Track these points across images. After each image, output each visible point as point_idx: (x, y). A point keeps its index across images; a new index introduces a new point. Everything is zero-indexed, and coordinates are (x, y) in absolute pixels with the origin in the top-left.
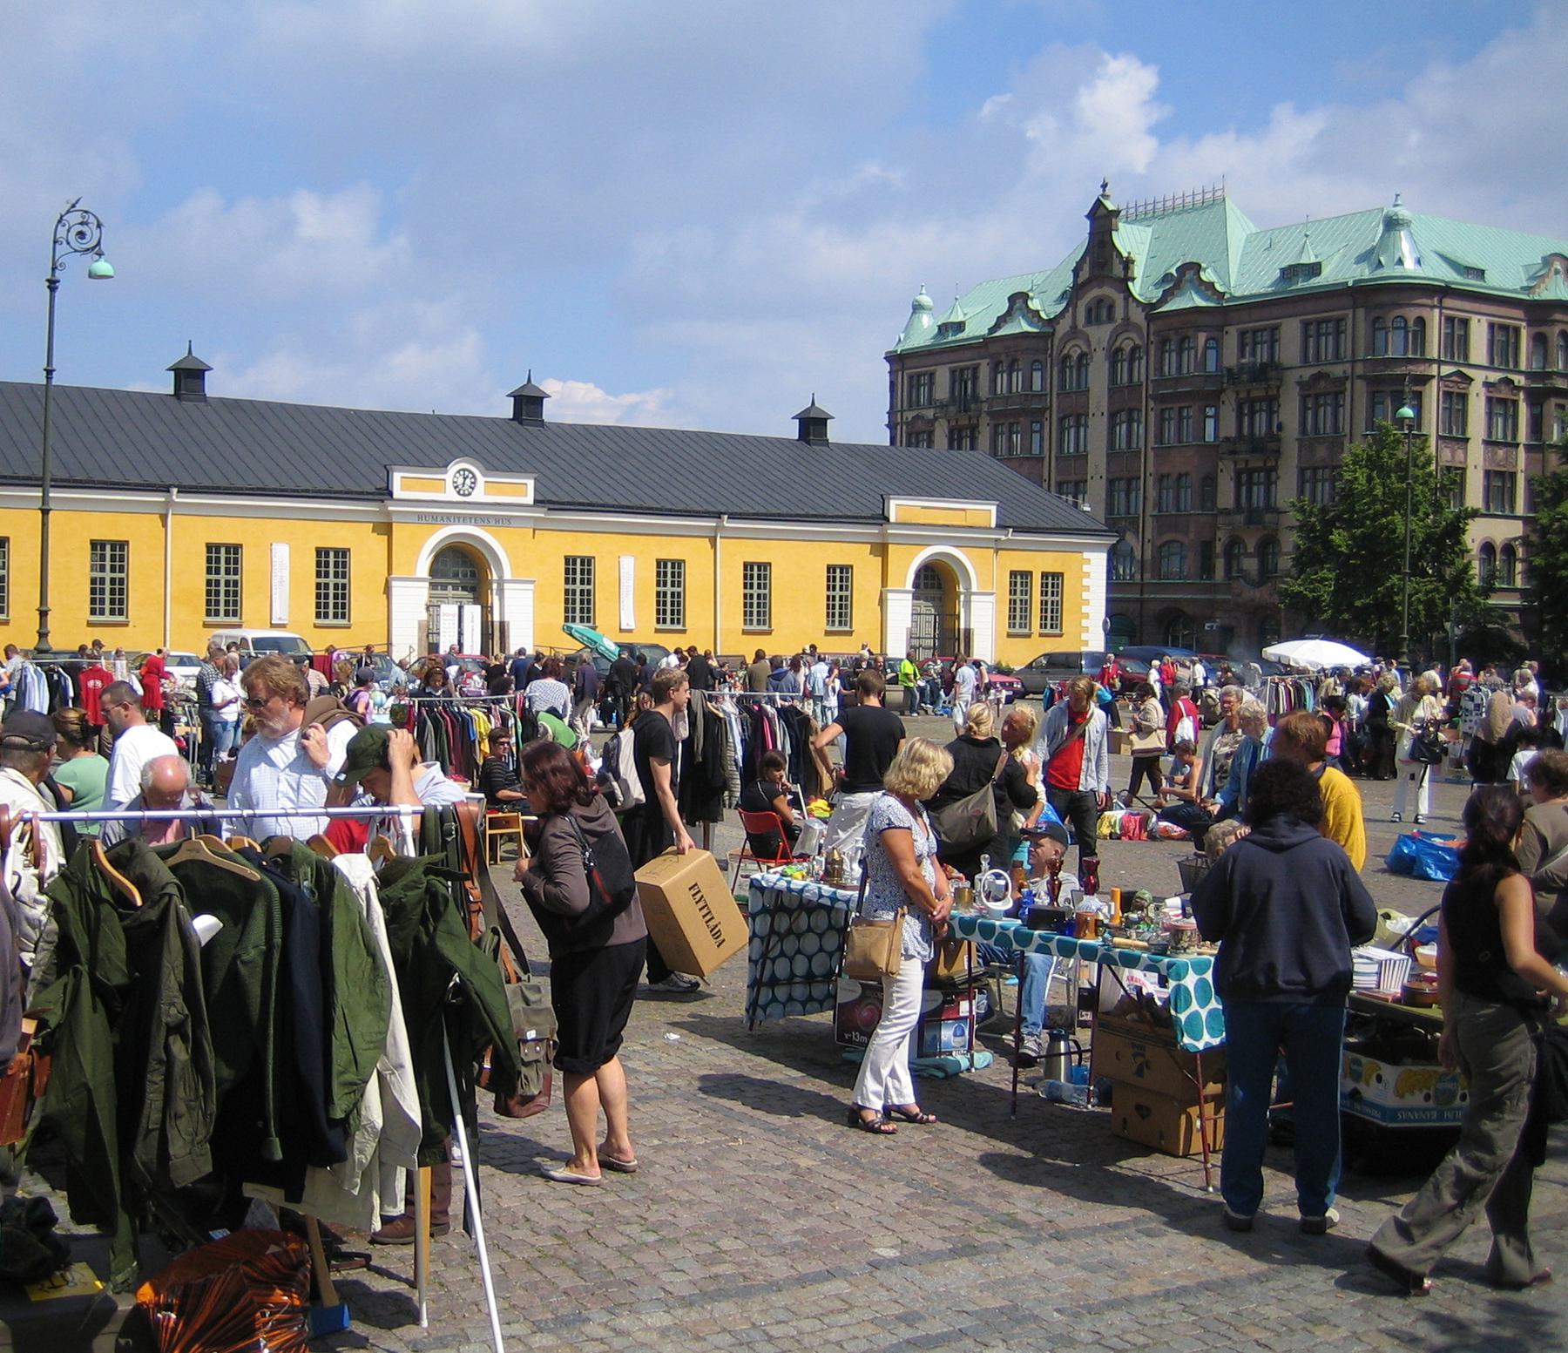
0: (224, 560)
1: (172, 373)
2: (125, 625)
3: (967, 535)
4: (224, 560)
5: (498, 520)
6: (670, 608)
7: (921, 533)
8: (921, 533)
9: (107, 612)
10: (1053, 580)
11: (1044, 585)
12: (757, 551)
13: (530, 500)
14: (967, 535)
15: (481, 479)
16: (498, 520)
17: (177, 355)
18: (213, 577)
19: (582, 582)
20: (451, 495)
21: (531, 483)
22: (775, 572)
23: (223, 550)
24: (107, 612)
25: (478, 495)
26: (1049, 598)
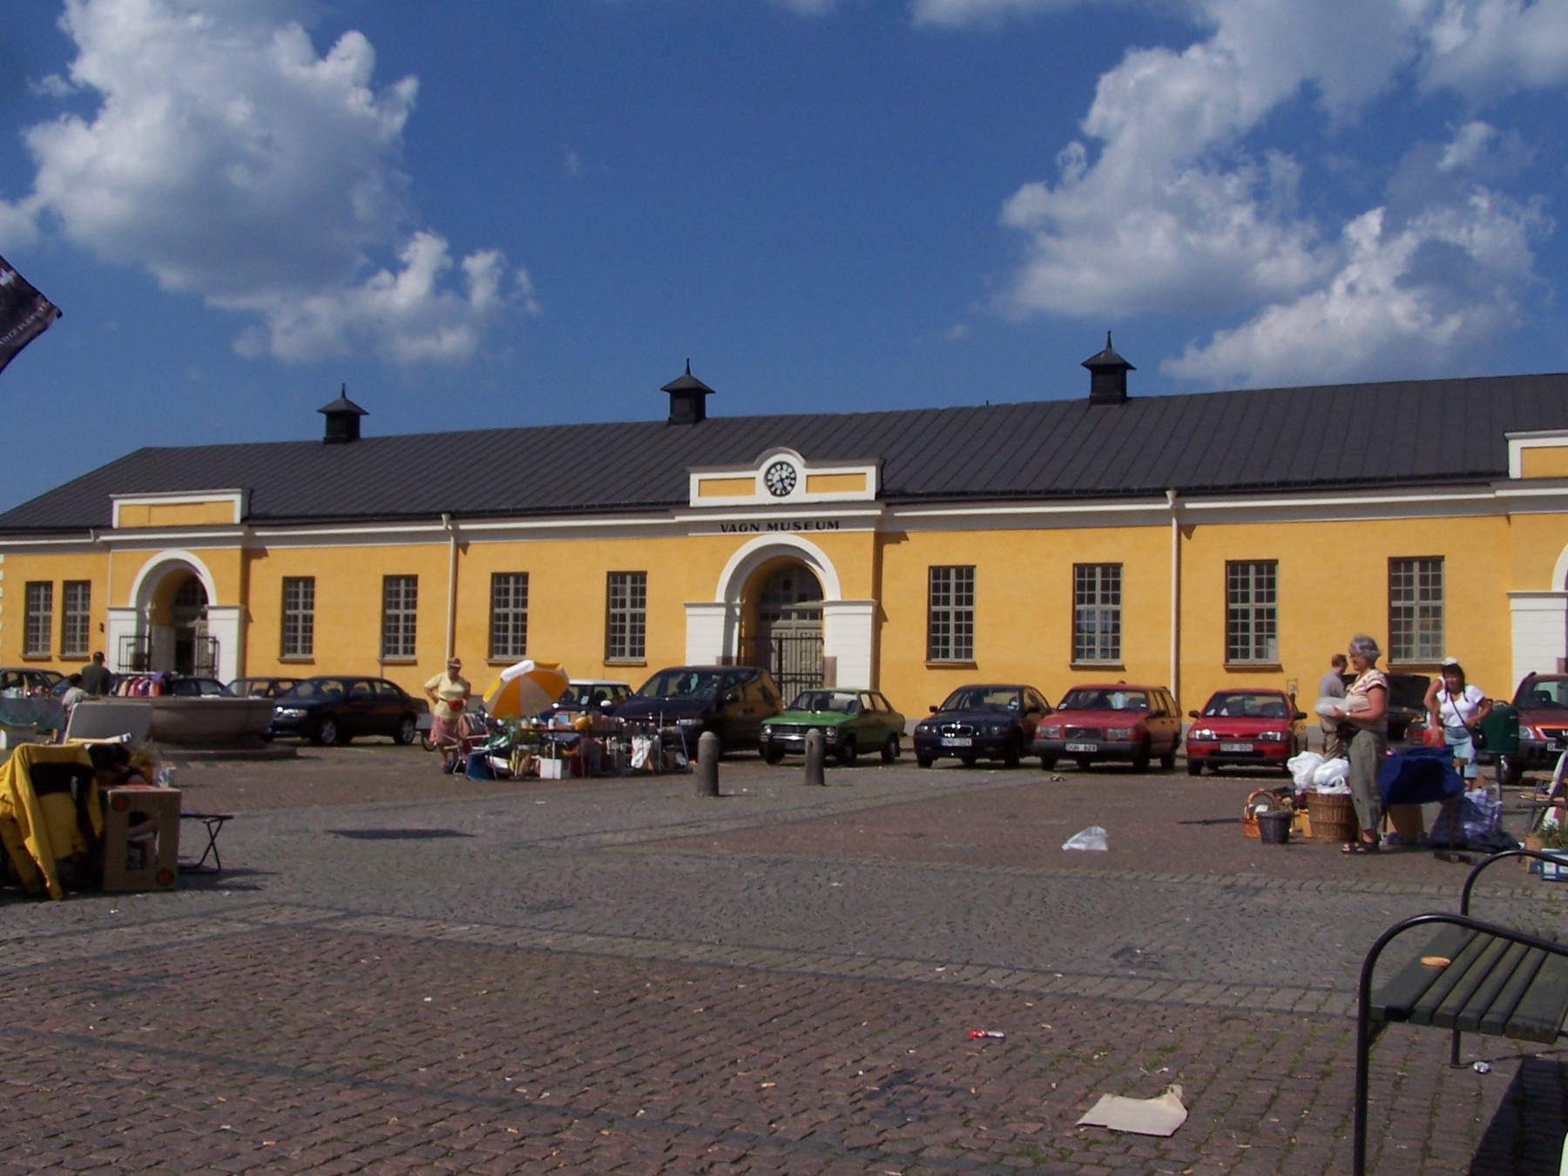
0: (509, 590)
1: (324, 416)
2: (414, 663)
3: (205, 535)
4: (509, 590)
5: (818, 524)
6: (398, 635)
7: (146, 537)
8: (146, 537)
9: (952, 653)
10: (78, 590)
11: (66, 597)
12: (1248, 542)
13: (869, 493)
14: (205, 535)
15: (802, 470)
16: (818, 524)
17: (674, 374)
18: (1265, 605)
19: (516, 605)
20: (763, 496)
21: (871, 472)
22: (1282, 575)
23: (1252, 569)
24: (952, 653)
25: (798, 494)
26: (301, 612)
